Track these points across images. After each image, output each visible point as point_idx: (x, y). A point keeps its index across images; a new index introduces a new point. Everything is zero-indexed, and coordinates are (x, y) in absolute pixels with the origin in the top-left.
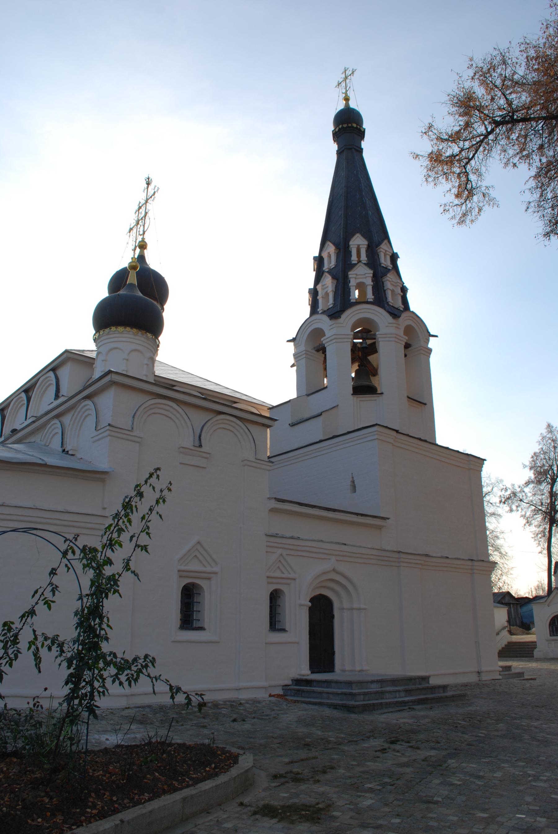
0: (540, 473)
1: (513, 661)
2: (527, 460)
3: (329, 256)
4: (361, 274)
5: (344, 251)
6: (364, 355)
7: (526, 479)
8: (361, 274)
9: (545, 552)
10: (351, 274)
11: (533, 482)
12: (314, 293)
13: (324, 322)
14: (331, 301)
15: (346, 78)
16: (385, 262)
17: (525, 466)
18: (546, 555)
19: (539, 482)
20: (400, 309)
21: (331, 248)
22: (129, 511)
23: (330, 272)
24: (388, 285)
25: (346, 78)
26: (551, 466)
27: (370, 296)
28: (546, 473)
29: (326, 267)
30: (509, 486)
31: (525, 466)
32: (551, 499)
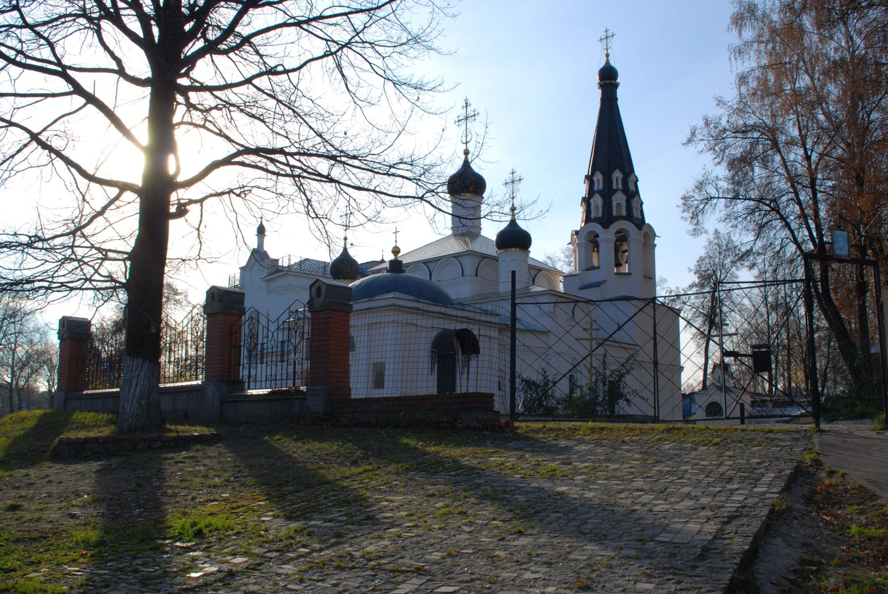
0: (701, 277)
1: (459, 444)
2: (693, 264)
3: (598, 181)
4: (619, 198)
5: (608, 180)
6: (622, 238)
7: (690, 282)
9: (703, 352)
10: (614, 198)
11: (696, 286)
12: (586, 201)
13: (597, 228)
14: (600, 214)
15: (607, 38)
16: (632, 187)
17: (690, 270)
18: (703, 356)
19: (702, 286)
20: (640, 223)
21: (599, 177)
22: (877, 525)
23: (599, 192)
25: (607, 38)
26: (714, 272)
27: (624, 213)
28: (709, 277)
29: (596, 188)
30: (673, 288)
31: (690, 270)
32: (712, 303)
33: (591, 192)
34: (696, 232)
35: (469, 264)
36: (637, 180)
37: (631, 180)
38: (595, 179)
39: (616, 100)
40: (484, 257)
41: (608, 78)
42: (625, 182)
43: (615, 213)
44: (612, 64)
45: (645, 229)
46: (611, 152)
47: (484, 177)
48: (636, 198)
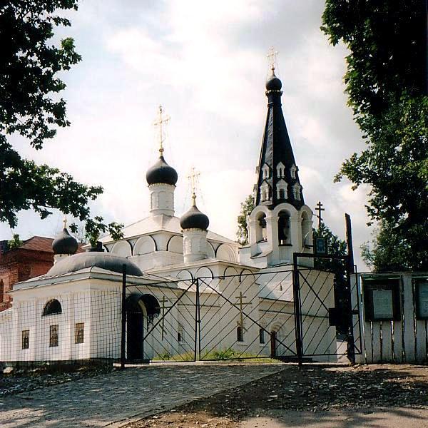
6: (284, 221)
8: (282, 185)
10: (277, 185)
16: (293, 176)
20: (299, 204)
24: (295, 190)
27: (286, 197)
29: (264, 177)
33: (260, 182)
34: (327, 230)
35: (162, 242)
36: (298, 170)
37: (293, 168)
38: (263, 169)
39: (425, 27)
40: (174, 235)
41: (274, 89)
42: (287, 171)
43: (278, 197)
44: (278, 77)
45: (303, 209)
46: (278, 146)
47: (174, 168)
48: (296, 185)
